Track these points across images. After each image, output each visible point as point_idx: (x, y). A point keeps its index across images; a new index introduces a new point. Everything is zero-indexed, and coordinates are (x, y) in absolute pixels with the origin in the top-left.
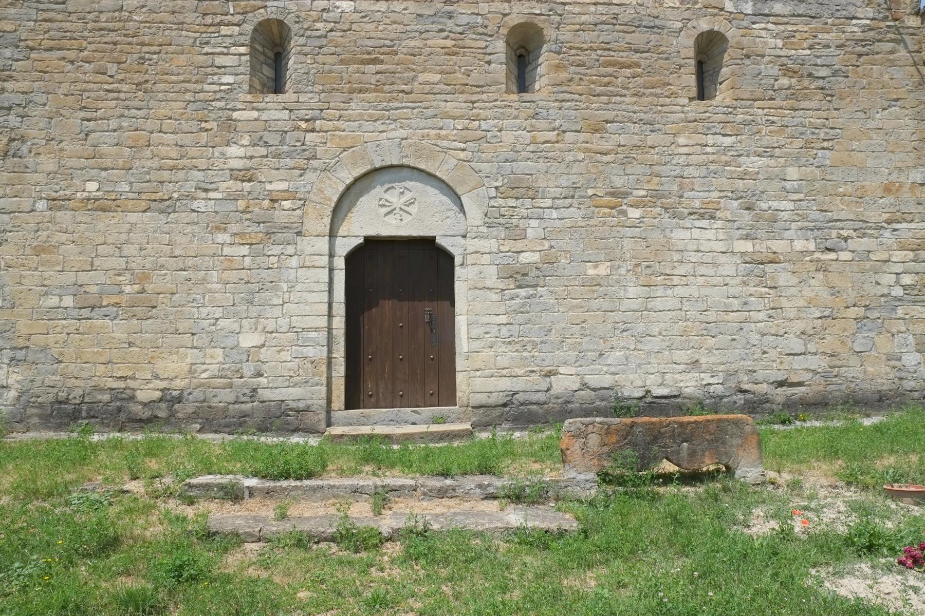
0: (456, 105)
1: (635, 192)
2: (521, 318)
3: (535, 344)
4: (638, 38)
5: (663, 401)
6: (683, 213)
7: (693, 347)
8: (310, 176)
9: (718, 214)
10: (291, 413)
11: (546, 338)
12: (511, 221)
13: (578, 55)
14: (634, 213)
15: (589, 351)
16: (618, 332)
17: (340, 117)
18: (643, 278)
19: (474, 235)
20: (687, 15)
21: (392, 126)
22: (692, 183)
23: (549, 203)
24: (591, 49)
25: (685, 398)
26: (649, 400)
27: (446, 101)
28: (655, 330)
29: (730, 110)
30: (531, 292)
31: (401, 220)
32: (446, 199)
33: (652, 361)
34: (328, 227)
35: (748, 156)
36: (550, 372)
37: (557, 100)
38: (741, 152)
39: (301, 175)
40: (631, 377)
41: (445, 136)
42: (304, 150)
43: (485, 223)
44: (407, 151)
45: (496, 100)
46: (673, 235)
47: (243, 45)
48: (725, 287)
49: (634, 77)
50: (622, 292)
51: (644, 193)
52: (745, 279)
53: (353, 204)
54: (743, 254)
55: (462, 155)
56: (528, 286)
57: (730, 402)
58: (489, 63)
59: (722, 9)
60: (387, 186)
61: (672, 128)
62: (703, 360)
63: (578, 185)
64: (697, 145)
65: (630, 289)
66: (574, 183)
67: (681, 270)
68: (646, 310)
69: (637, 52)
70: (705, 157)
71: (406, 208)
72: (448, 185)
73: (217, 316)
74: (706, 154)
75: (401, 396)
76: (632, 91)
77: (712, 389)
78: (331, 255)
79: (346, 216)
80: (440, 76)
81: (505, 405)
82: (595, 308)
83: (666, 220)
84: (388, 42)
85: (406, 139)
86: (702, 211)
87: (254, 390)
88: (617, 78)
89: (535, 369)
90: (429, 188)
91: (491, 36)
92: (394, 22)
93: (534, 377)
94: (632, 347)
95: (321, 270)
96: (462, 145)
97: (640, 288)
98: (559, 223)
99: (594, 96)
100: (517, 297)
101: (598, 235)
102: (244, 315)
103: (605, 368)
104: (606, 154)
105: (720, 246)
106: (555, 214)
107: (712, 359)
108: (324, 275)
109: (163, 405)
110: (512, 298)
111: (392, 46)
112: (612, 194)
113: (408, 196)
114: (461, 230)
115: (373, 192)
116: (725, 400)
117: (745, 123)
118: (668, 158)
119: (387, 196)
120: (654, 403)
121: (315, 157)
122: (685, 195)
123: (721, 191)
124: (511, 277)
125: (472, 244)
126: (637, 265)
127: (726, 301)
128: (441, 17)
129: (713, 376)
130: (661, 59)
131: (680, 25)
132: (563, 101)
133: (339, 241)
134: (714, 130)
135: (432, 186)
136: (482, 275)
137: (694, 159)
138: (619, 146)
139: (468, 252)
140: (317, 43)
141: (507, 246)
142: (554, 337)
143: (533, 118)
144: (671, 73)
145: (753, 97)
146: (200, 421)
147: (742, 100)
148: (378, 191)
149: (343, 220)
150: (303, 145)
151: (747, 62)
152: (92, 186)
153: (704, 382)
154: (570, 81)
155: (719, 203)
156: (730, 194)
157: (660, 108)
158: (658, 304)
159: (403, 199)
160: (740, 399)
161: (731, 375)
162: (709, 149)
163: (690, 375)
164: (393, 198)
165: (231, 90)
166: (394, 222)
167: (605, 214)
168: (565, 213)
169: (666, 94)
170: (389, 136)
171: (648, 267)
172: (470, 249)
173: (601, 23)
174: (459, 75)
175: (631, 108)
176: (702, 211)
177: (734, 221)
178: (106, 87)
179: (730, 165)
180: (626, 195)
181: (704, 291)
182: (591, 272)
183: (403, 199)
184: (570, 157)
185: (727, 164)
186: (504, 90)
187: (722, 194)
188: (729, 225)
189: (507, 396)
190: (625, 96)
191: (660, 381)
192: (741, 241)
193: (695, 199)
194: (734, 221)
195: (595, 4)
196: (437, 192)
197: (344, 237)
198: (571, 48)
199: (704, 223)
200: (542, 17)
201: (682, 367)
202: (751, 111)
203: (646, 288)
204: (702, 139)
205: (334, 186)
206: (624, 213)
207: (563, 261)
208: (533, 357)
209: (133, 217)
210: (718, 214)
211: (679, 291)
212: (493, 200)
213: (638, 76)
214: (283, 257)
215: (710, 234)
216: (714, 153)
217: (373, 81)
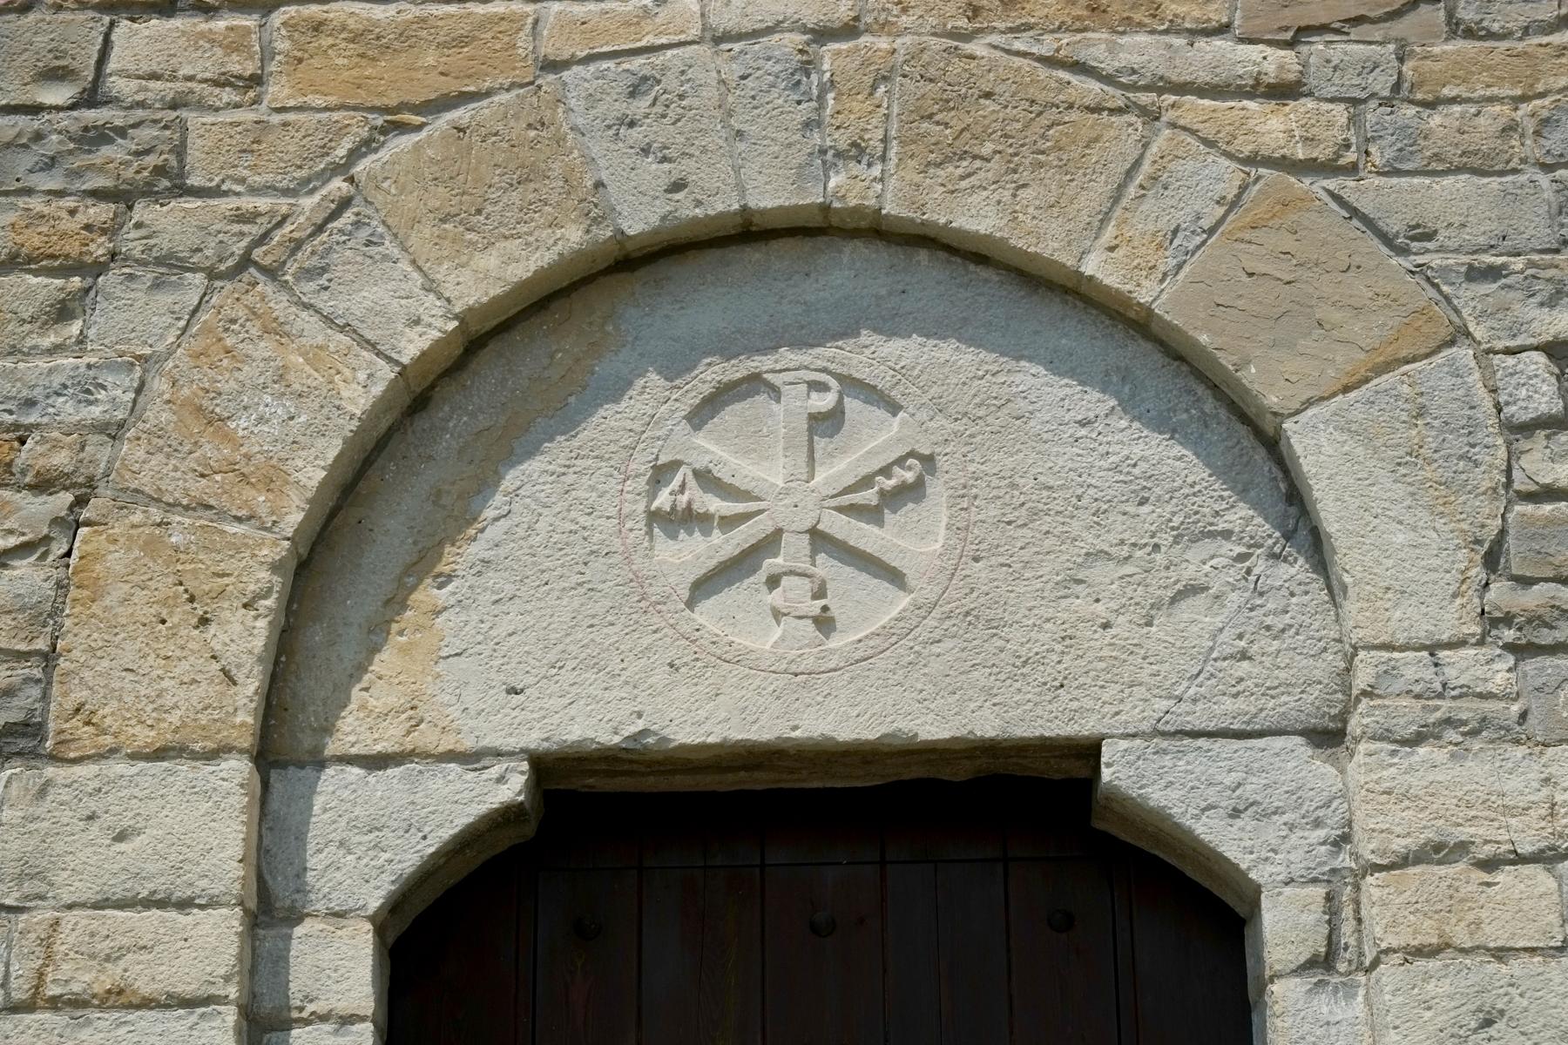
8: (132, 314)
19: (1408, 715)
31: (824, 623)
32: (1170, 460)
34: (250, 686)
39: (62, 312)
42: (97, 137)
43: (1492, 621)
44: (858, 117)
53: (455, 515)
55: (1273, 126)
60: (712, 373)
71: (863, 535)
72: (1178, 354)
78: (270, 908)
79: (396, 602)
85: (850, 30)
90: (1031, 377)
95: (177, 1022)
96: (1273, 62)
113: (874, 439)
114: (1296, 678)
115: (609, 422)
119: (709, 448)
121: (172, 182)
125: (1393, 791)
133: (336, 797)
135: (1057, 364)
139: (1368, 849)
148: (642, 415)
149: (376, 635)
150: (91, 97)
159: (839, 466)
164: (765, 461)
166: (767, 639)
172: (1387, 827)
183: (839, 466)
196: (1095, 402)
197: (376, 762)
205: (304, 375)
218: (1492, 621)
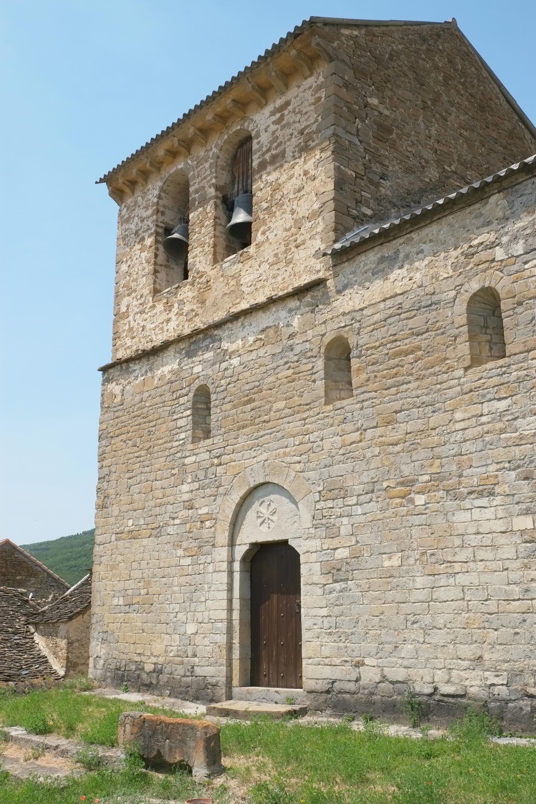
0: (294, 426)
1: (421, 479)
2: (337, 610)
3: (347, 636)
4: (418, 322)
5: (451, 700)
6: (462, 493)
7: (476, 641)
8: (219, 500)
9: (498, 489)
10: (210, 687)
11: (355, 629)
12: (330, 521)
13: (373, 354)
14: (420, 500)
15: (387, 643)
16: (409, 624)
17: (233, 451)
18: (428, 567)
20: (459, 281)
21: (260, 452)
22: (471, 459)
23: (354, 500)
24: (382, 345)
25: (470, 698)
26: (437, 697)
27: (289, 423)
28: (440, 621)
29: (504, 369)
30: (343, 586)
31: (269, 528)
33: (439, 656)
35: (524, 417)
36: (359, 663)
37: (359, 402)
38: (516, 415)
40: (421, 671)
41: (289, 453)
43: (313, 525)
45: (319, 414)
46: (454, 519)
47: (189, 409)
48: (505, 573)
49: (416, 362)
50: (411, 582)
51: (427, 477)
52: (526, 561)
53: (244, 518)
54: (523, 532)
56: (341, 580)
57: (515, 707)
58: (314, 381)
59: (493, 260)
60: (261, 500)
61: (450, 404)
62: (486, 657)
63: (376, 480)
64: (473, 416)
65: (418, 579)
66: (372, 478)
67: (462, 556)
68: (432, 600)
69: (418, 335)
70: (479, 428)
73: (177, 610)
74: (482, 424)
75: (282, 677)
76: (415, 377)
77: (496, 690)
80: (285, 402)
81: (328, 692)
82: (390, 600)
83: (450, 504)
84: (257, 384)
85: (267, 460)
86: (481, 488)
87: (193, 667)
88: (403, 366)
89: (347, 659)
90: (283, 498)
91: (316, 357)
92: (260, 366)
93: (348, 667)
94: (421, 640)
96: (297, 459)
97: (426, 578)
98: (362, 518)
99: (386, 389)
100: (334, 590)
101: (392, 526)
102: (188, 610)
103: (400, 661)
104: (396, 445)
105: (499, 526)
106: (359, 510)
107: (495, 656)
108: (224, 578)
109: (155, 675)
110: (331, 592)
111: (259, 386)
112: (402, 484)
116: (510, 705)
117: (519, 381)
118: (447, 437)
120: (442, 701)
121: (220, 486)
122: (465, 473)
123: (497, 463)
124: (330, 572)
126: (423, 554)
127: (507, 588)
128: (286, 351)
129: (497, 676)
130: (438, 335)
131: (453, 293)
132: (363, 401)
134: (489, 396)
136: (311, 572)
137: (470, 433)
138: (407, 434)
140: (222, 396)
141: (328, 543)
142: (360, 629)
143: (343, 423)
144: (448, 347)
145: (526, 349)
146: (169, 688)
147: (515, 354)
150: (216, 476)
151: (520, 309)
152: (130, 522)
153: (489, 683)
154: (368, 380)
155: (496, 476)
156: (507, 465)
157: (439, 386)
158: (441, 594)
160: (526, 705)
161: (517, 675)
162: (484, 419)
163: (474, 673)
165: (184, 443)
167: (397, 504)
168: (367, 507)
169: (444, 370)
170: (258, 460)
171: (432, 555)
173: (389, 317)
174: (296, 398)
175: (414, 393)
176: (481, 488)
177: (513, 495)
178: (136, 455)
179: (505, 432)
180: (412, 483)
181: (485, 578)
182: (387, 564)
184: (369, 455)
185: (503, 431)
186: (323, 403)
187: (499, 466)
188: (509, 500)
189: (328, 683)
190: (410, 382)
191: (447, 677)
192: (521, 518)
193: (473, 476)
194: (513, 495)
195: (384, 300)
197: (239, 545)
198: (367, 349)
199: (483, 502)
200: (347, 328)
201: (467, 663)
202: (525, 365)
203: (431, 577)
204: (476, 409)
206: (412, 501)
207: (365, 555)
208: (346, 647)
209: (145, 541)
210: (498, 489)
211: (461, 579)
212: (317, 504)
213: (419, 359)
214: (206, 564)
215: (489, 513)
216: (489, 423)
217: (249, 418)
218: (313, 525)
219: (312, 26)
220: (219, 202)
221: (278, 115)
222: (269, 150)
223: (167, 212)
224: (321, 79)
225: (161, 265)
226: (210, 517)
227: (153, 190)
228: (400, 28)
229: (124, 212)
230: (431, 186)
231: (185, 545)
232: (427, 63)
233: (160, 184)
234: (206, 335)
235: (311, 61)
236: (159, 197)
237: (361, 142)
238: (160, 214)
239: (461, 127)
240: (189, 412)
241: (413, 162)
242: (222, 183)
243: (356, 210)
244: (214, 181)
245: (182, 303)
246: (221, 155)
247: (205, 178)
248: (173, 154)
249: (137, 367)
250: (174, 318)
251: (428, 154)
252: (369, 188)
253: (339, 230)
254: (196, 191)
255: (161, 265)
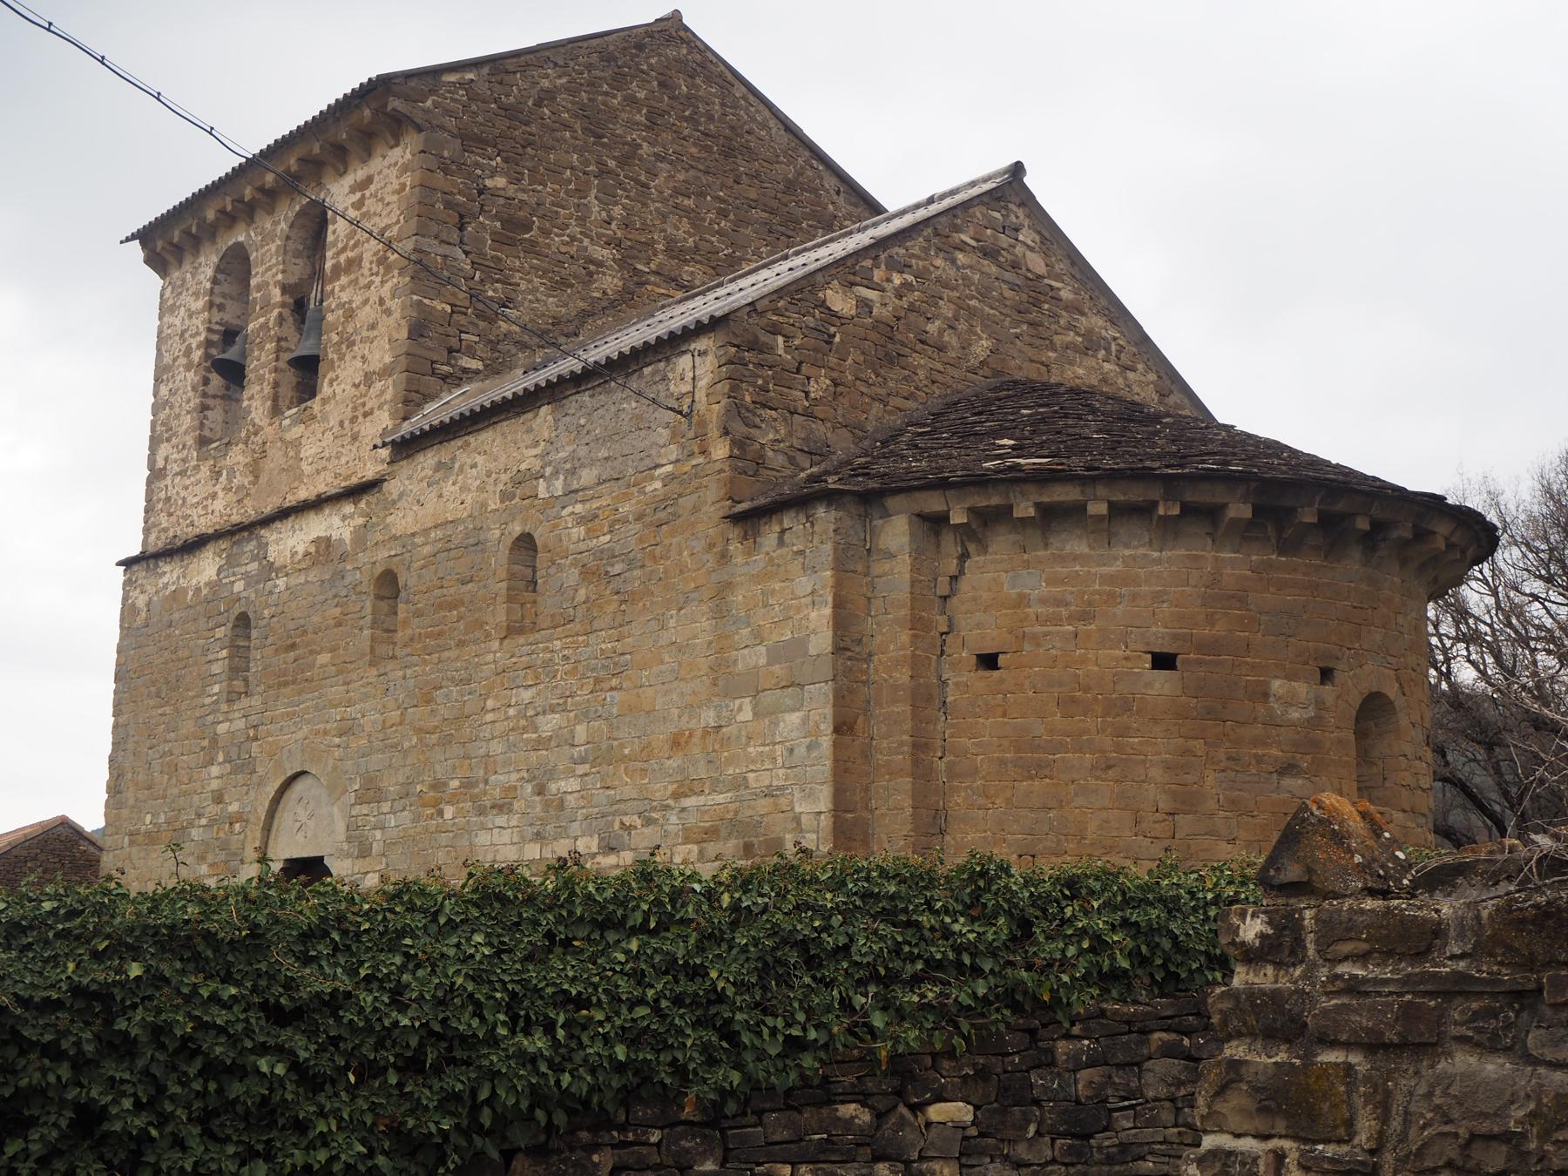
219: (378, 89)
220: (287, 312)
221: (358, 195)
222: (344, 249)
223: (229, 303)
224: (408, 156)
225: (214, 397)
226: (239, 817)
227: (207, 264)
228: (562, 50)
229: (168, 293)
230: (605, 304)
231: (210, 858)
232: (614, 97)
233: (215, 259)
234: (251, 533)
235: (396, 126)
236: (215, 281)
237: (466, 253)
238: (215, 310)
239: (677, 192)
240: (224, 653)
241: (570, 268)
242: (293, 280)
243: (448, 364)
244: (280, 277)
245: (232, 473)
246: (293, 235)
247: (269, 269)
248: (229, 219)
249: (167, 568)
250: (221, 494)
251: (601, 253)
252: (477, 326)
253: (411, 400)
254: (259, 288)
255: (214, 397)
